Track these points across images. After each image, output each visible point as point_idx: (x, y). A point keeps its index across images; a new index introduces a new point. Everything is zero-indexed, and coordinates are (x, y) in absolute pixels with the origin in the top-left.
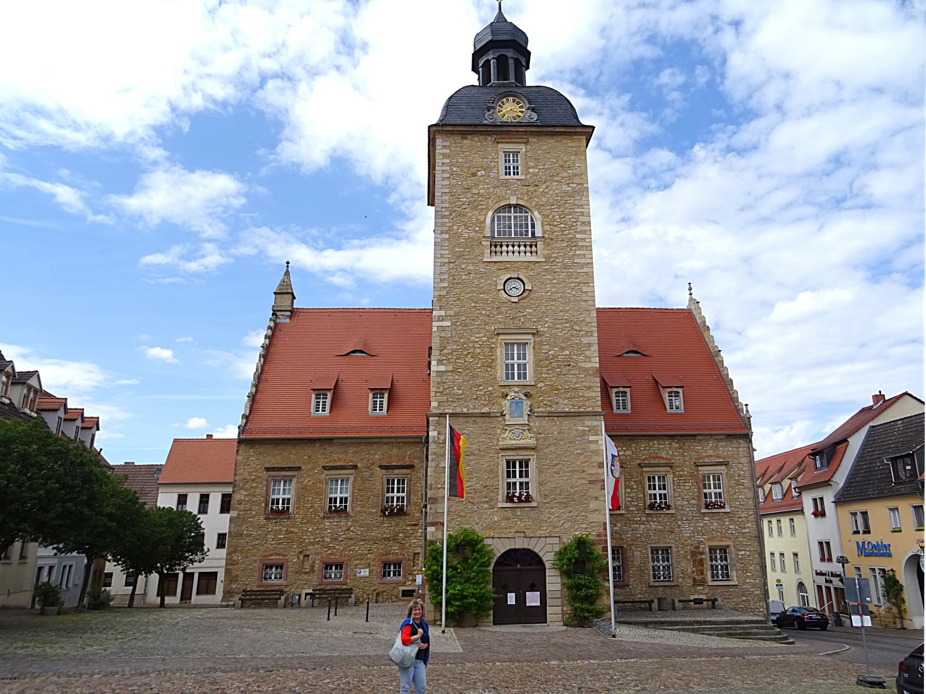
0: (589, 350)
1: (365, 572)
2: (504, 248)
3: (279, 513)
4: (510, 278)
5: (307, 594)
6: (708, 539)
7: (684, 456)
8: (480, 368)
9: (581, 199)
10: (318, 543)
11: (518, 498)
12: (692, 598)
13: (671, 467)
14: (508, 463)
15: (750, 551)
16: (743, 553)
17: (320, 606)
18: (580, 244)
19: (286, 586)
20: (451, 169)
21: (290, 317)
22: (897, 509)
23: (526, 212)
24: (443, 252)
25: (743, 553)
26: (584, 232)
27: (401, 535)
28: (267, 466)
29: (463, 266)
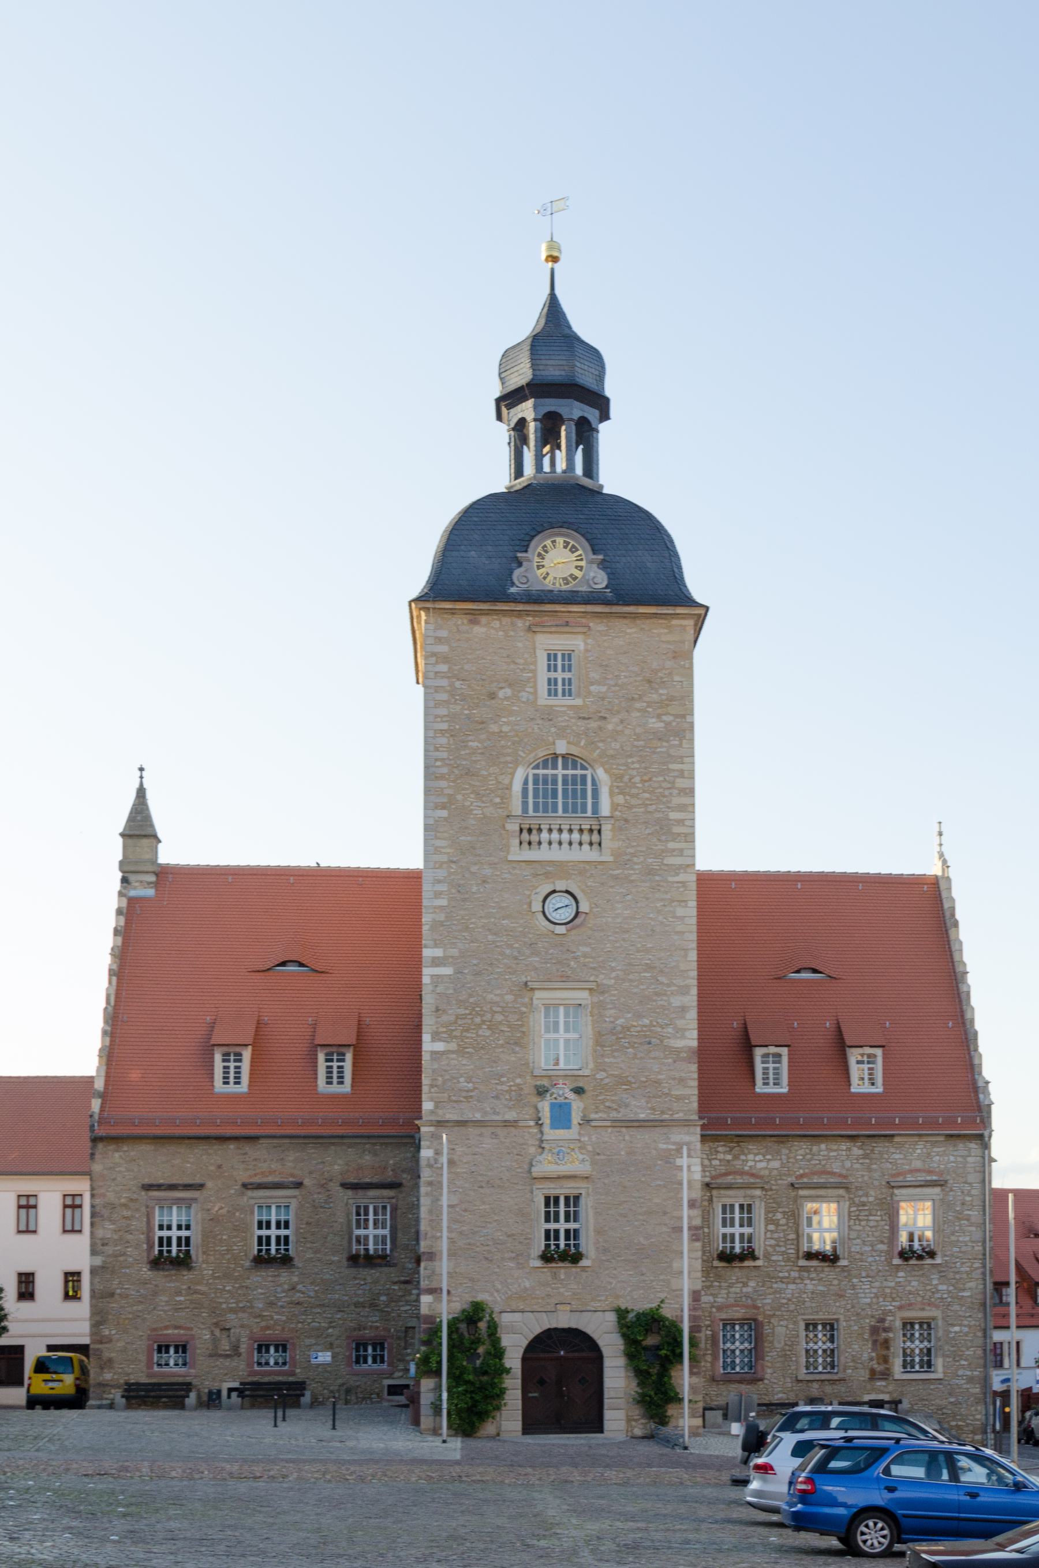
0: (683, 1018)
1: (325, 1357)
2: (545, 835)
3: (172, 1260)
4: (554, 892)
5: (230, 1390)
6: (900, 1308)
7: (870, 1170)
8: (502, 1046)
9: (680, 745)
10: (243, 1309)
11: (562, 1254)
12: (867, 1398)
13: (847, 1188)
14: (547, 1200)
15: (970, 1327)
16: (957, 1329)
18: (676, 830)
19: (195, 1376)
21: (156, 885)
23: (583, 768)
24: (439, 843)
25: (957, 1329)
28: (146, 1181)
29: (474, 869)
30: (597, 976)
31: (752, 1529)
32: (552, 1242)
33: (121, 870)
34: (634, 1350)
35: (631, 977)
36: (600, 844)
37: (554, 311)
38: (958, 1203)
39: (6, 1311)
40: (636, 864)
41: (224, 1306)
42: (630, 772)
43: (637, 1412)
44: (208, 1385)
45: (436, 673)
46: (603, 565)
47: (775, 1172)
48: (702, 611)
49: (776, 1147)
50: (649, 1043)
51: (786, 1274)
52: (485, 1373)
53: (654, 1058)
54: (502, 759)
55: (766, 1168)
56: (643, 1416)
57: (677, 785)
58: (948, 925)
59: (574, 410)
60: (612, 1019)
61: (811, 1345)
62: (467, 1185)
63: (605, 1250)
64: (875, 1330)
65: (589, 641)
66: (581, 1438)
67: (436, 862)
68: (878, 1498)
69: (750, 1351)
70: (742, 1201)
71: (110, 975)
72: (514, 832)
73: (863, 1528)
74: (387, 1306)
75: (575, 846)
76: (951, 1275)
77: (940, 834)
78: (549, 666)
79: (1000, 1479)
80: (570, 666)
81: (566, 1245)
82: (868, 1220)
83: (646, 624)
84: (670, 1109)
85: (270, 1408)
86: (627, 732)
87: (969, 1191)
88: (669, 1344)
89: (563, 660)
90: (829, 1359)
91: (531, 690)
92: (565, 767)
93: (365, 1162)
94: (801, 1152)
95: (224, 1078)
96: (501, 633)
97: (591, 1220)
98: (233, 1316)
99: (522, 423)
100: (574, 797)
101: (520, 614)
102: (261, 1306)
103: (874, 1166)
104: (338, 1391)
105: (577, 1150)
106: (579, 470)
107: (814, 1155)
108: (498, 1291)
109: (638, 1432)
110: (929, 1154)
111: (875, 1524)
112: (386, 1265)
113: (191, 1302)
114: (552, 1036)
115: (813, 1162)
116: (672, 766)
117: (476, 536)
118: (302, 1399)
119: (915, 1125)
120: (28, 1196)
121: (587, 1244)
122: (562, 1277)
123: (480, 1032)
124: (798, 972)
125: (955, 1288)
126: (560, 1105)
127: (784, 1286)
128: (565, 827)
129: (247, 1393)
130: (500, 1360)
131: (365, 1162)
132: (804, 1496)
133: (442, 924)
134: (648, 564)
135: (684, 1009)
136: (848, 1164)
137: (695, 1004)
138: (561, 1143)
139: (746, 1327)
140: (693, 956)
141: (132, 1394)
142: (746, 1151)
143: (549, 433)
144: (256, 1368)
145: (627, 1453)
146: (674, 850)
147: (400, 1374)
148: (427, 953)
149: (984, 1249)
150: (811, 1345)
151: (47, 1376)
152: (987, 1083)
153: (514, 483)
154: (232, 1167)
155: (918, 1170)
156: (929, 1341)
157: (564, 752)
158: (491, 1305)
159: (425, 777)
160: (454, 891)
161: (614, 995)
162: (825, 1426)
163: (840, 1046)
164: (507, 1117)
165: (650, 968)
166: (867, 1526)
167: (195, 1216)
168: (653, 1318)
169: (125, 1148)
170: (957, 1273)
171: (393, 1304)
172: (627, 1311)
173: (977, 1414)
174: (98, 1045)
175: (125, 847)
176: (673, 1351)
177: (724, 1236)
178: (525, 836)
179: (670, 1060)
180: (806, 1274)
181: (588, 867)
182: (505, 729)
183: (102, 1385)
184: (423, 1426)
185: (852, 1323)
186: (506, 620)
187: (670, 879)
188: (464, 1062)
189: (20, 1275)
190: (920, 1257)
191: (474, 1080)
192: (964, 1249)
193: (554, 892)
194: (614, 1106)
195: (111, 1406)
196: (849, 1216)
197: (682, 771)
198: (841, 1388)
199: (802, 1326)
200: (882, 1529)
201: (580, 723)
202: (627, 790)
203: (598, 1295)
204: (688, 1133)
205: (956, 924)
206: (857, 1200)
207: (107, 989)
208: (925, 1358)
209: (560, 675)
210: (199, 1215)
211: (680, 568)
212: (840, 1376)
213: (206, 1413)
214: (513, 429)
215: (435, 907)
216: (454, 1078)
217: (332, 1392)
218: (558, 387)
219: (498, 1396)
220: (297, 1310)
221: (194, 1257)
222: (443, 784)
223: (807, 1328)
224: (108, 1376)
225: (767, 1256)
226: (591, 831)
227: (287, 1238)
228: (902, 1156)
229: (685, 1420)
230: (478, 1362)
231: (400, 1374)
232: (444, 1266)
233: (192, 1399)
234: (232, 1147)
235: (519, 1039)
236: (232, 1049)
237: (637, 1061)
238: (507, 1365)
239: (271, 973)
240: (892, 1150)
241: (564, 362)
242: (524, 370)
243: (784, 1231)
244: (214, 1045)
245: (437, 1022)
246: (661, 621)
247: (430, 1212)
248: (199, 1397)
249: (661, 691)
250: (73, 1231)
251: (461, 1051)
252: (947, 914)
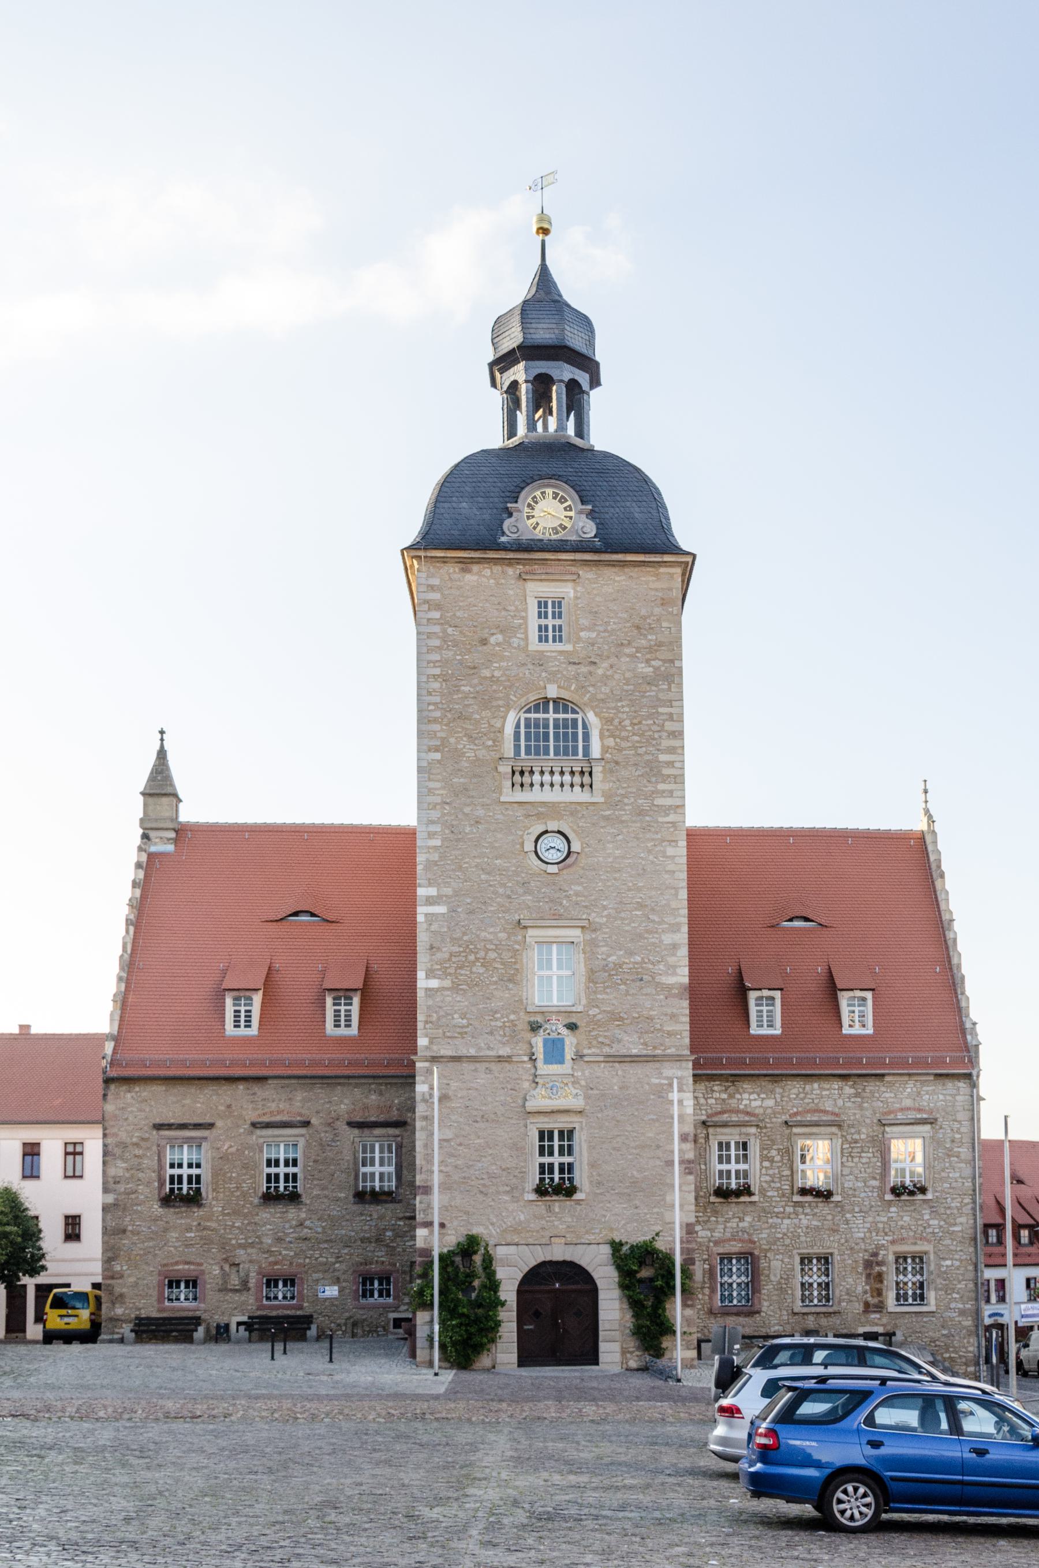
0: (674, 955)
2: (537, 777)
3: (181, 1196)
4: (546, 832)
5: (239, 1324)
6: (893, 1242)
8: (496, 983)
9: (669, 689)
11: (556, 1187)
12: (861, 1330)
13: (839, 1126)
14: (542, 1134)
15: (961, 1261)
16: (949, 1263)
17: (261, 1339)
18: (666, 771)
19: (205, 1311)
20: (444, 631)
21: (176, 841)
23: (574, 712)
24: (432, 785)
25: (949, 1263)
26: (672, 750)
27: (389, 1234)
28: (158, 1121)
29: (467, 810)
30: (589, 914)
31: (715, 1483)
32: (546, 1176)
33: (141, 827)
34: (628, 1281)
35: (623, 915)
36: (591, 786)
37: (544, 278)
38: (948, 1140)
39: (44, 1251)
40: (626, 805)
41: (234, 1242)
42: (620, 715)
43: (632, 1344)
44: (220, 1319)
45: (428, 620)
46: (591, 515)
47: (769, 1111)
48: (689, 559)
49: (770, 1086)
50: (641, 980)
51: (782, 1210)
52: (480, 1306)
53: (646, 994)
54: (495, 703)
55: (761, 1106)
56: (638, 1348)
57: (666, 728)
58: (935, 876)
59: (565, 372)
60: (604, 957)
61: (806, 1278)
62: (461, 1120)
63: (599, 1184)
64: (868, 1264)
65: (579, 589)
66: (575, 1370)
67: (429, 804)
68: (856, 1454)
69: (747, 1284)
70: (737, 1138)
71: (127, 925)
72: (506, 773)
73: (839, 1495)
75: (567, 787)
76: (942, 1211)
77: (926, 792)
78: (540, 613)
79: (1013, 1431)
80: (560, 613)
81: (560, 1178)
82: (860, 1157)
83: (634, 572)
84: (662, 1045)
85: (267, 1341)
86: (617, 676)
87: (959, 1129)
88: (663, 1276)
89: (553, 607)
90: (824, 1293)
91: (522, 636)
92: (556, 711)
93: (372, 1102)
94: (795, 1091)
95: (235, 1021)
96: (492, 581)
97: (585, 1153)
98: (242, 1252)
99: (514, 385)
100: (566, 740)
101: (510, 562)
103: (866, 1105)
104: (345, 1324)
105: (570, 1085)
106: (571, 430)
107: (807, 1094)
108: (492, 1224)
109: (633, 1364)
110: (919, 1093)
111: (856, 1489)
112: (391, 1202)
114: (546, 973)
115: (806, 1101)
116: (660, 710)
117: (467, 488)
118: (308, 1333)
119: (905, 1064)
120: (75, 1144)
121: (581, 1177)
122: (557, 1210)
123: (474, 969)
124: (791, 920)
125: (946, 1223)
126: (553, 1041)
127: (779, 1221)
128: (557, 770)
129: (256, 1326)
130: (496, 1292)
131: (372, 1102)
132: (765, 1454)
133: (435, 863)
134: (636, 515)
135: (675, 947)
136: (840, 1102)
137: (686, 941)
138: (554, 1078)
139: (742, 1261)
140: (684, 894)
141: (142, 1328)
142: (741, 1090)
143: (541, 397)
144: (265, 1302)
145: (618, 1385)
146: (664, 791)
147: (406, 1307)
148: (421, 892)
149: (974, 1185)
150: (806, 1278)
151: (63, 1312)
152: (975, 1024)
153: (506, 443)
155: (909, 1109)
156: (922, 1275)
157: (555, 696)
158: (486, 1237)
159: (418, 720)
160: (447, 831)
161: (605, 933)
162: (807, 1361)
163: (832, 989)
164: (501, 1053)
165: (641, 906)
166: (845, 1492)
167: (205, 1155)
168: (646, 1250)
169: (137, 1089)
170: (949, 1208)
171: (398, 1239)
172: (621, 1244)
173: (971, 1346)
174: (113, 989)
175: (146, 805)
176: (667, 1284)
177: (721, 1172)
178: (517, 778)
179: (662, 997)
180: (800, 1210)
181: (579, 808)
182: (497, 674)
184: (418, 1359)
185: (846, 1257)
186: (497, 569)
187: (660, 819)
188: (458, 999)
189: (67, 1217)
190: (912, 1193)
191: (468, 1016)
192: (954, 1185)
193: (546, 832)
194: (607, 1041)
195: (122, 1341)
196: (842, 1153)
197: (671, 714)
198: (836, 1321)
199: (797, 1260)
200: (865, 1495)
201: (571, 668)
202: (618, 733)
203: (593, 1228)
204: (680, 1068)
205: (942, 876)
206: (849, 1137)
207: (124, 938)
208: (918, 1292)
209: (550, 622)
210: (209, 1154)
211: (667, 519)
212: (835, 1308)
213: (213, 1346)
214: (506, 392)
215: (429, 847)
216: (448, 1014)
217: (339, 1325)
218: (548, 353)
219: (493, 1328)
220: (304, 1246)
222: (436, 727)
223: (802, 1262)
224: (119, 1311)
225: (763, 1192)
226: (582, 773)
227: (295, 1175)
228: (892, 1095)
229: (679, 1351)
230: (474, 1295)
231: (406, 1307)
232: (436, 1198)
233: (200, 1333)
234: (241, 1087)
235: (513, 976)
236: (242, 994)
237: (629, 997)
238: (502, 1298)
239: (284, 922)
240: (883, 1089)
241: (554, 326)
242: (516, 334)
243: (779, 1167)
245: (431, 960)
246: (648, 569)
247: (426, 1146)
248: (208, 1330)
249: (650, 637)
251: (455, 988)
252: (934, 866)
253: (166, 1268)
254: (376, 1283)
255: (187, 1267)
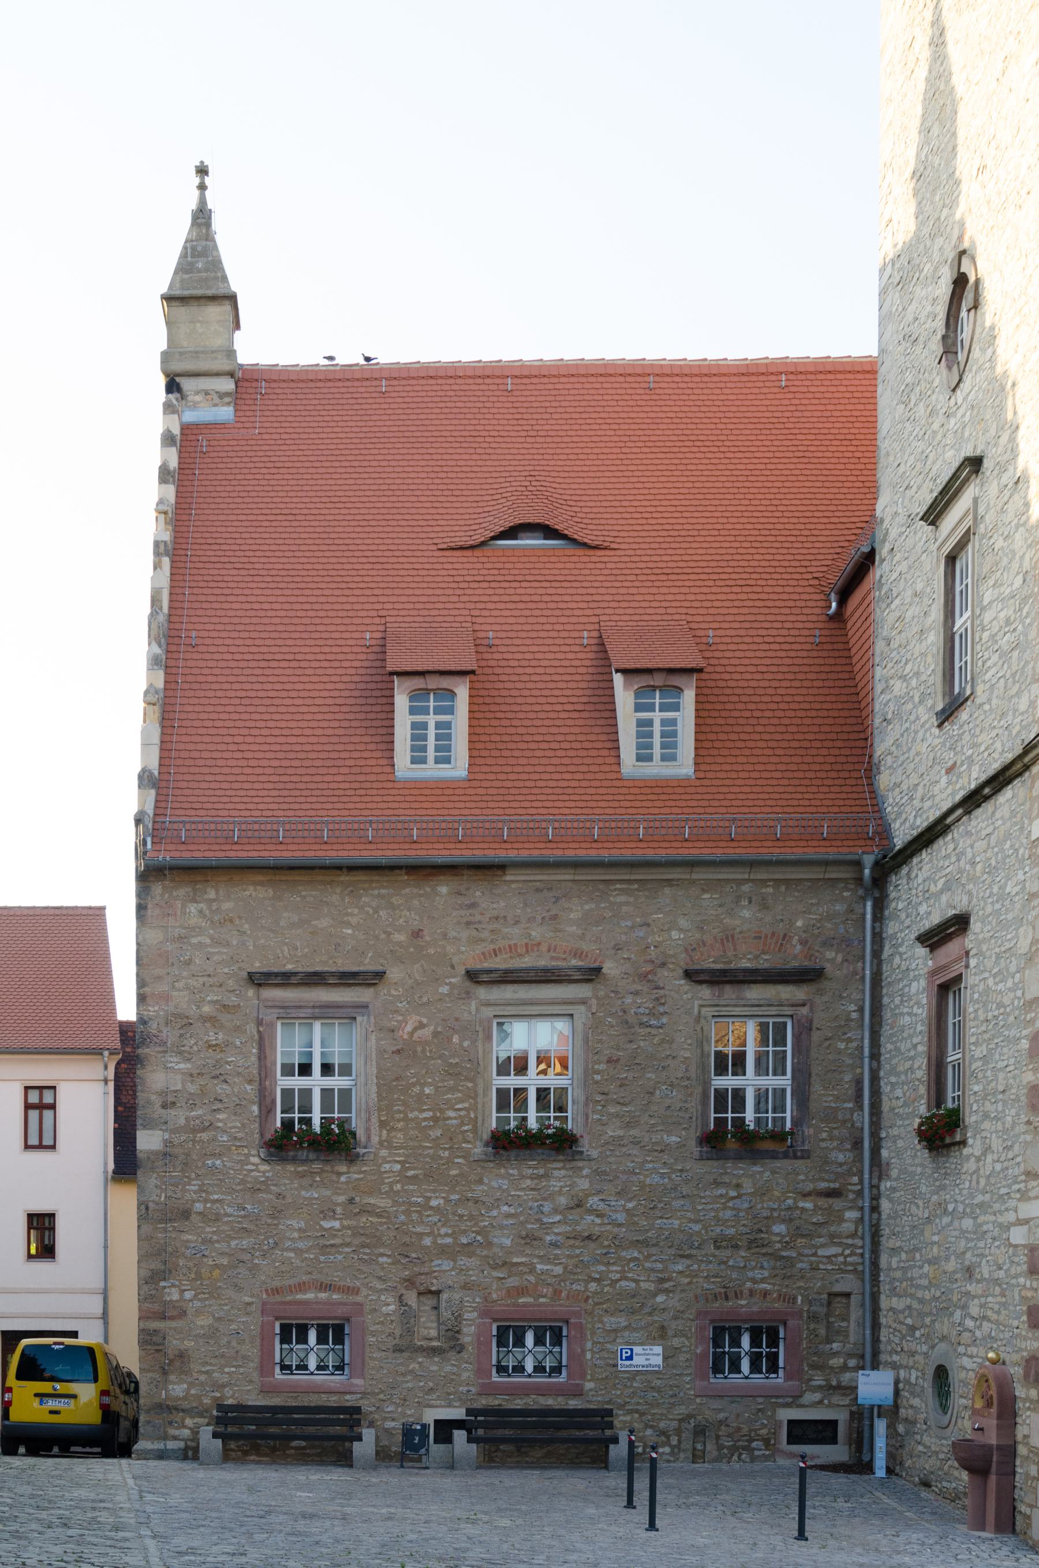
1: (649, 1357)
3: (311, 1143)
10: (468, 1249)
22: (54, 1088)
27: (780, 1228)
28: (257, 966)
41: (427, 1241)
71: (157, 553)
74: (787, 1245)
93: (743, 923)
98: (447, 1265)
102: (508, 1242)
104: (678, 1432)
112: (786, 1156)
113: (356, 1232)
131: (743, 923)
144: (496, 1378)
147: (817, 1396)
151: (45, 1387)
154: (445, 935)
169: (212, 894)
183: (166, 1409)
195: (190, 1453)
217: (663, 1433)
221: (361, 1134)
224: (177, 1389)
231: (817, 1396)
233: (365, 1447)
234: (444, 890)
236: (433, 682)
239: (487, 551)
244: (392, 674)
250: (41, 1147)
253: (278, 1298)
254: (746, 1341)
255: (323, 1295)
